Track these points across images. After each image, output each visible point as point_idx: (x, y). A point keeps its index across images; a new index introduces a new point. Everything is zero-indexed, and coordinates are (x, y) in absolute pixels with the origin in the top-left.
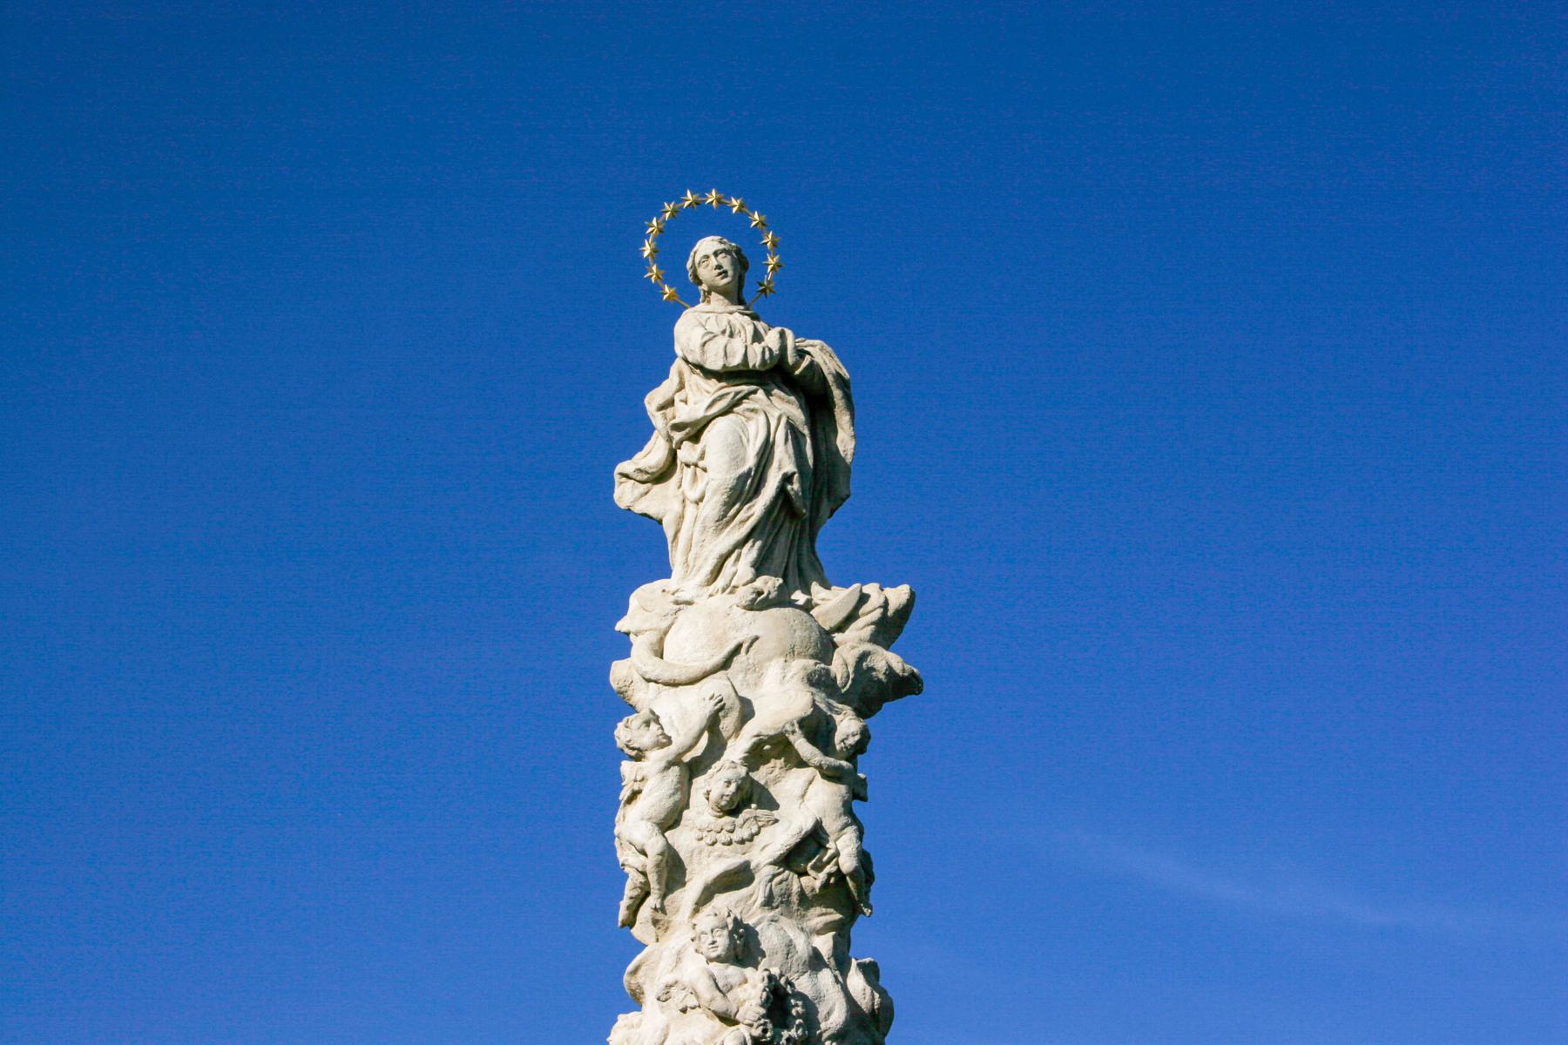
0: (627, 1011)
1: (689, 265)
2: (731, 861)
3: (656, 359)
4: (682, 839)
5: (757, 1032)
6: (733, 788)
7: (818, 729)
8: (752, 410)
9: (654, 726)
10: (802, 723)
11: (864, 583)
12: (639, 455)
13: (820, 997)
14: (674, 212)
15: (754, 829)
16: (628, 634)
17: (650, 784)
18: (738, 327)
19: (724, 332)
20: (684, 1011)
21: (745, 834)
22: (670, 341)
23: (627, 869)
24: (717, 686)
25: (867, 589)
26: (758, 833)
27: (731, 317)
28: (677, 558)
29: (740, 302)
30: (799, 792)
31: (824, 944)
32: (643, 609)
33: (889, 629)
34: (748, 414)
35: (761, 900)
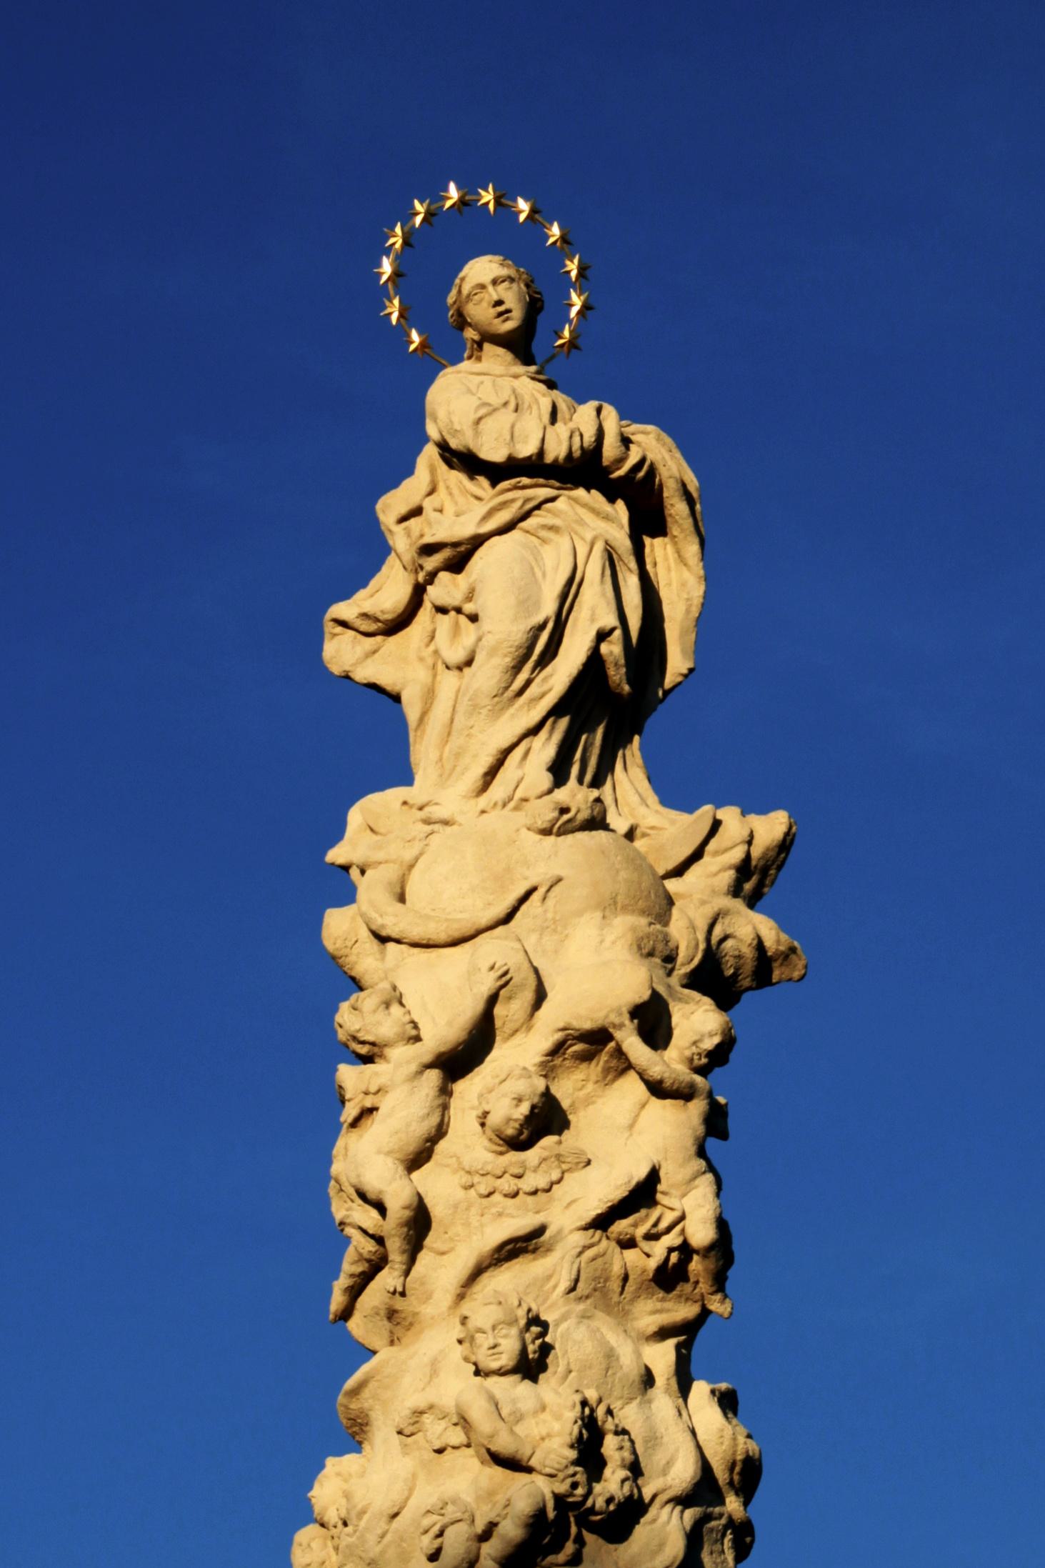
0: (340, 1453)
1: (451, 299)
2: (517, 1223)
3: (397, 436)
4: (437, 1184)
5: (562, 1488)
6: (524, 1109)
7: (652, 1020)
8: (551, 528)
9: (395, 1008)
10: (638, 1012)
11: (719, 805)
12: (362, 594)
13: (654, 1440)
14: (429, 215)
15: (555, 1176)
16: (346, 868)
17: (396, 1096)
18: (527, 399)
19: (506, 404)
20: (440, 1451)
21: (542, 1182)
22: (417, 414)
23: (349, 1231)
24: (495, 951)
25: (721, 814)
26: (559, 1181)
27: (516, 383)
28: (424, 753)
29: (527, 359)
30: (624, 1120)
31: (662, 1357)
32: (371, 830)
33: (752, 881)
34: (543, 533)
35: (565, 1284)
